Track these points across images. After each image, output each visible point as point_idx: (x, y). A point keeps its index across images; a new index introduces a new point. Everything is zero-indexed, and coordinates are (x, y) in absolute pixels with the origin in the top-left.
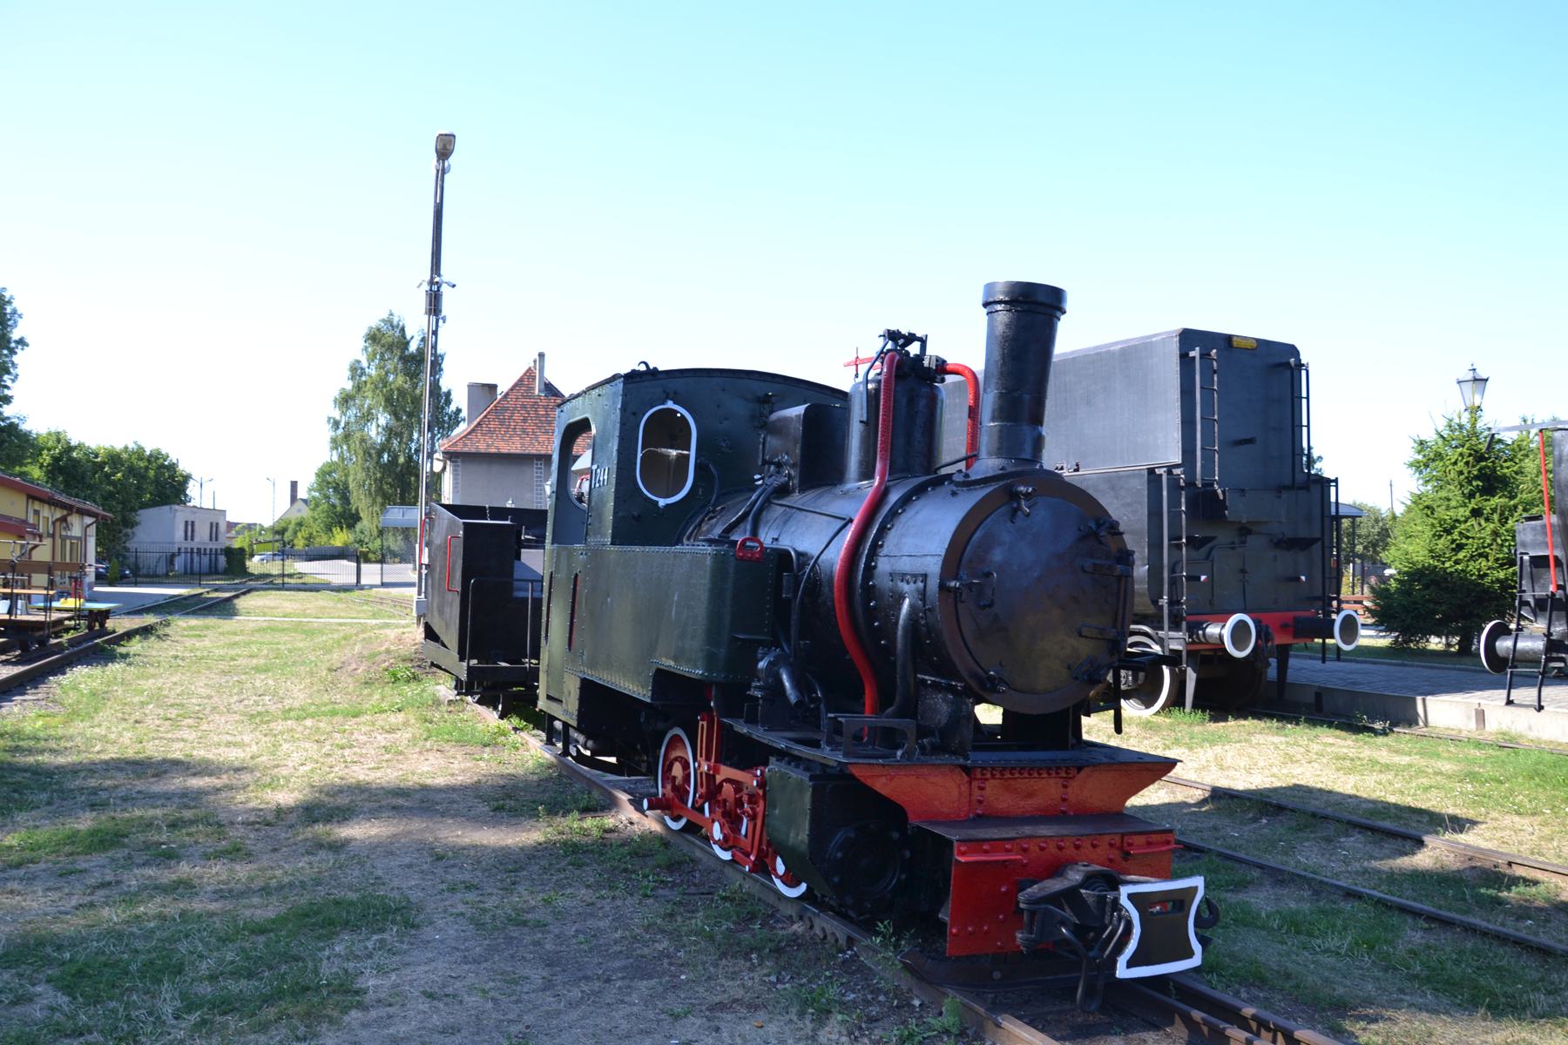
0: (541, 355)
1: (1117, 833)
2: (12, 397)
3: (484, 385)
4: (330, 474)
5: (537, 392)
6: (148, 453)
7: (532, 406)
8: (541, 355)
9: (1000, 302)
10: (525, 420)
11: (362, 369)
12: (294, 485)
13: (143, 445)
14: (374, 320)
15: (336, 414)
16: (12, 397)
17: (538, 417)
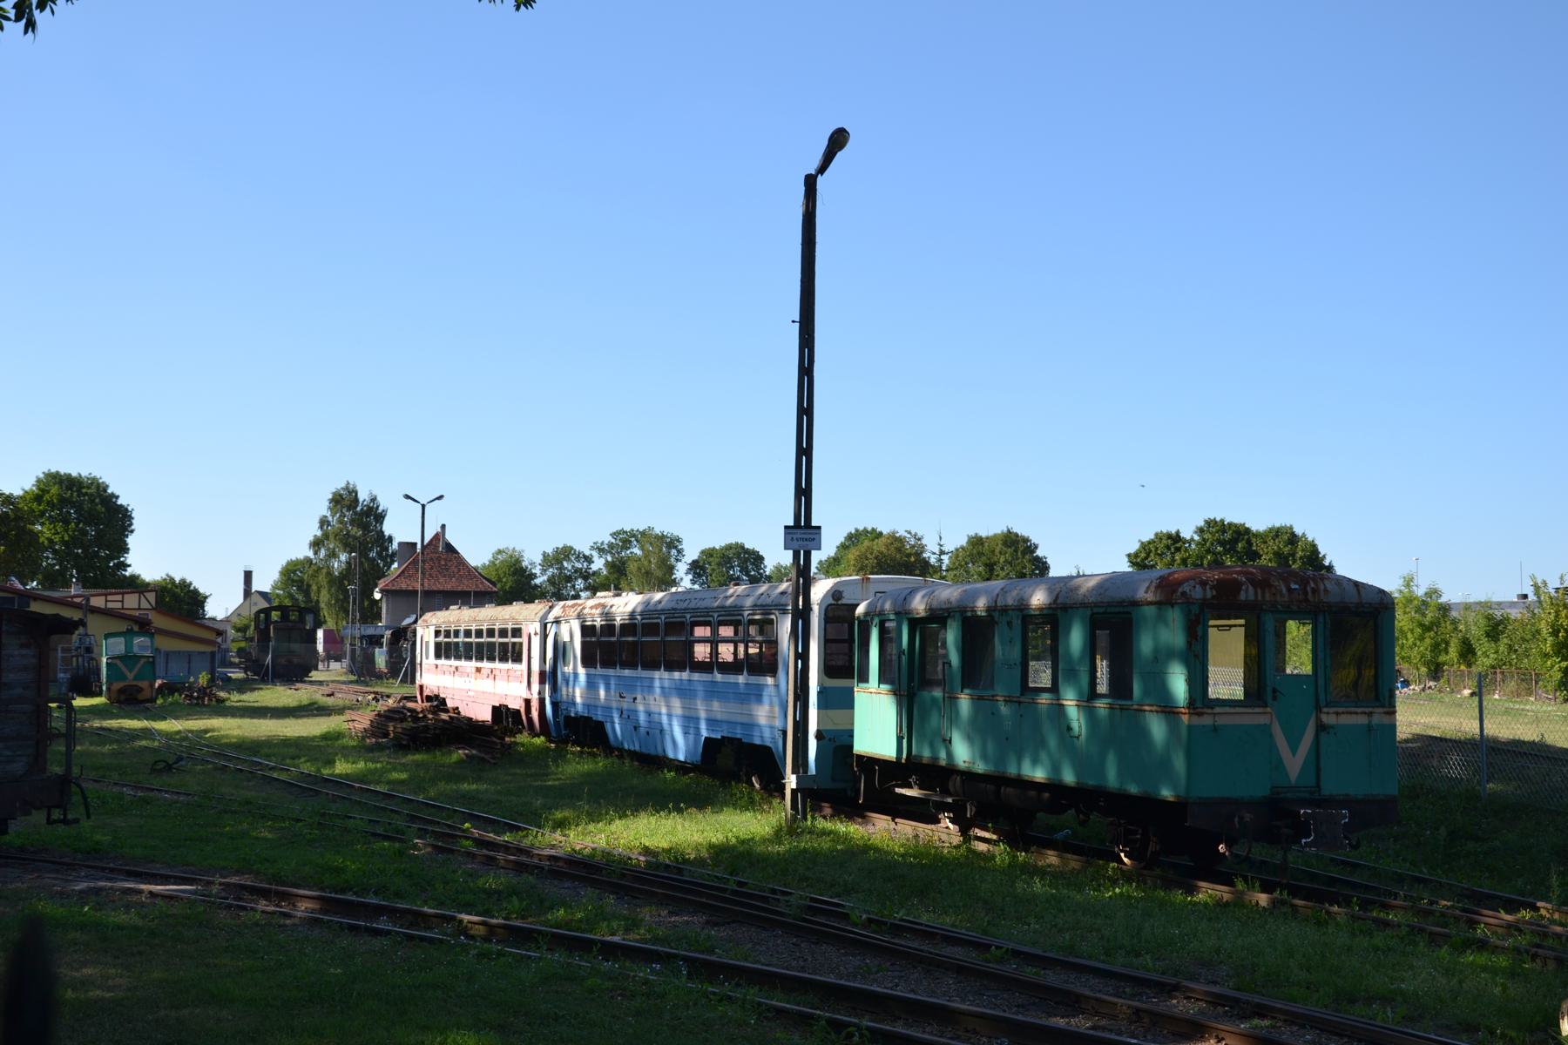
0: (443, 527)
3: (408, 543)
4: (294, 572)
5: (440, 549)
6: (177, 582)
8: (443, 527)
10: (432, 568)
12: (248, 576)
13: (173, 575)
17: (440, 566)
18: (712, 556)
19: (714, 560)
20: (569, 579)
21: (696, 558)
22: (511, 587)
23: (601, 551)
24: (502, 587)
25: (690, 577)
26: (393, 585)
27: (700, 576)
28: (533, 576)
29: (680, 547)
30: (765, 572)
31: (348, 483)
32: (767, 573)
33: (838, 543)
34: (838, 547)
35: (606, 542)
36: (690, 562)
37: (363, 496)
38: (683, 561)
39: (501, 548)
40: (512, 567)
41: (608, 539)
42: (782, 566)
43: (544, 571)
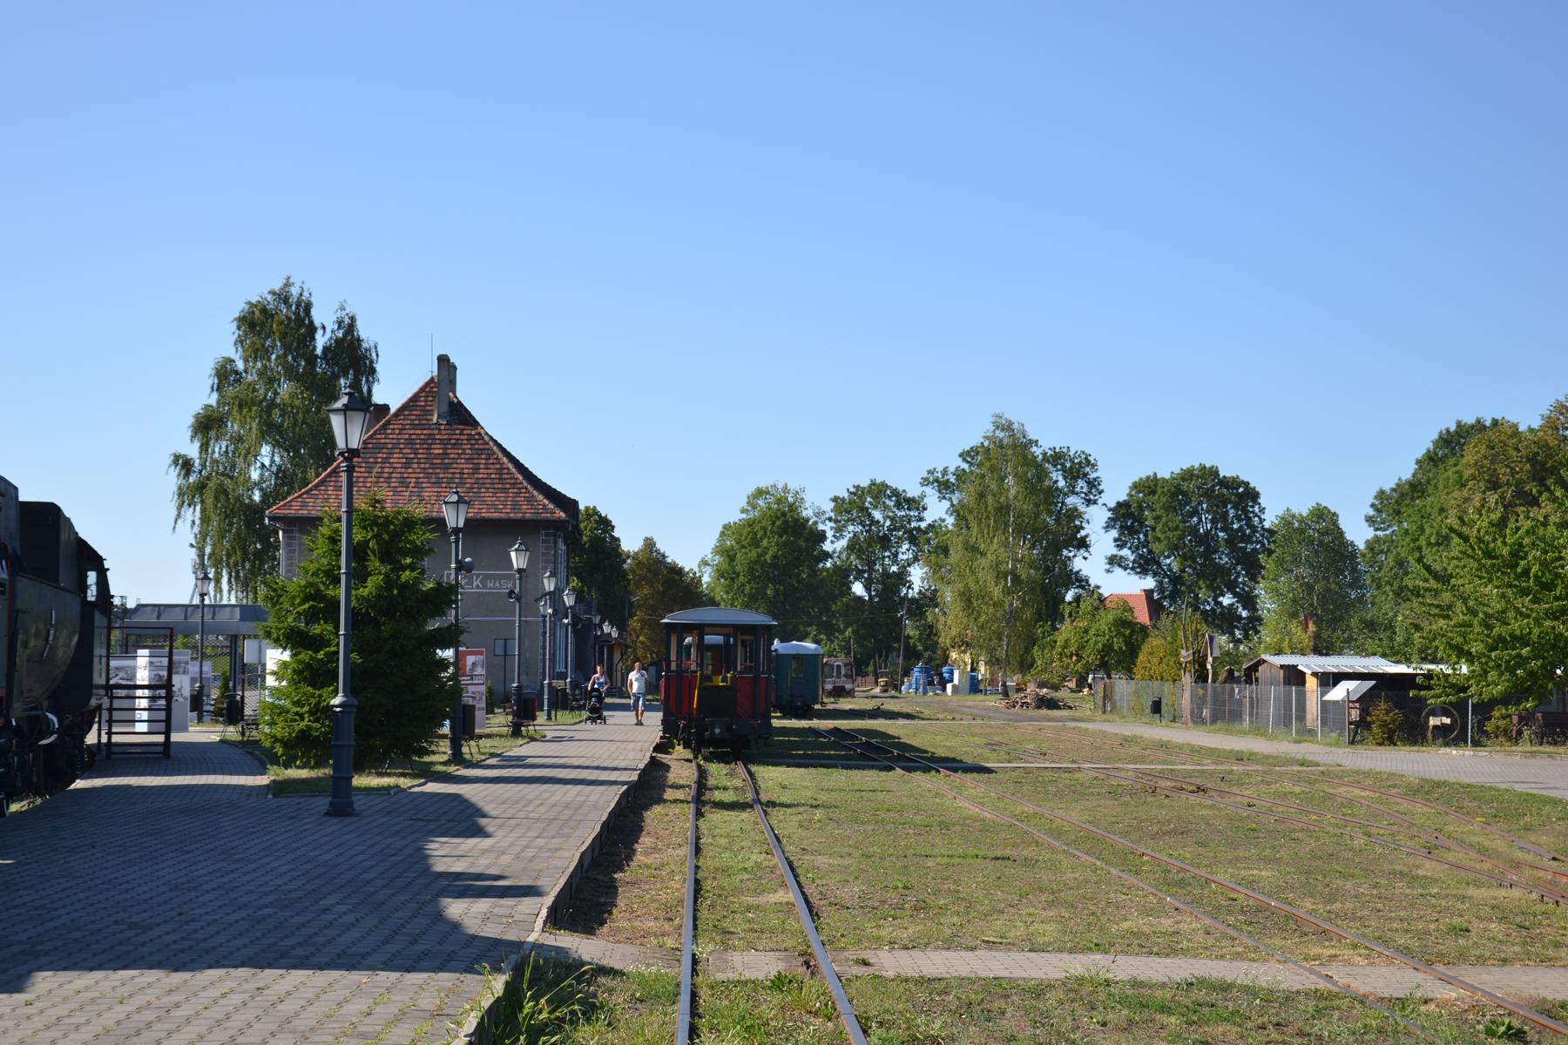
1: (566, 667)
2: (1493, 419)
7: (424, 442)
8: (443, 361)
9: (140, 697)
10: (407, 465)
11: (237, 373)
14: (259, 289)
15: (192, 450)
16: (1493, 419)
17: (429, 457)
18: (1153, 492)
19: (1159, 500)
20: (885, 542)
21: (1123, 497)
22: (775, 557)
23: (944, 487)
24: (759, 556)
25: (1114, 533)
26: (304, 505)
27: (1132, 531)
28: (822, 537)
29: (1093, 476)
30: (1261, 521)
31: (288, 284)
32: (1267, 525)
33: (1420, 453)
34: (1418, 462)
35: (952, 469)
36: (1112, 504)
37: (325, 317)
38: (1100, 502)
39: (763, 485)
40: (778, 518)
41: (955, 463)
42: (1293, 516)
43: (839, 531)
